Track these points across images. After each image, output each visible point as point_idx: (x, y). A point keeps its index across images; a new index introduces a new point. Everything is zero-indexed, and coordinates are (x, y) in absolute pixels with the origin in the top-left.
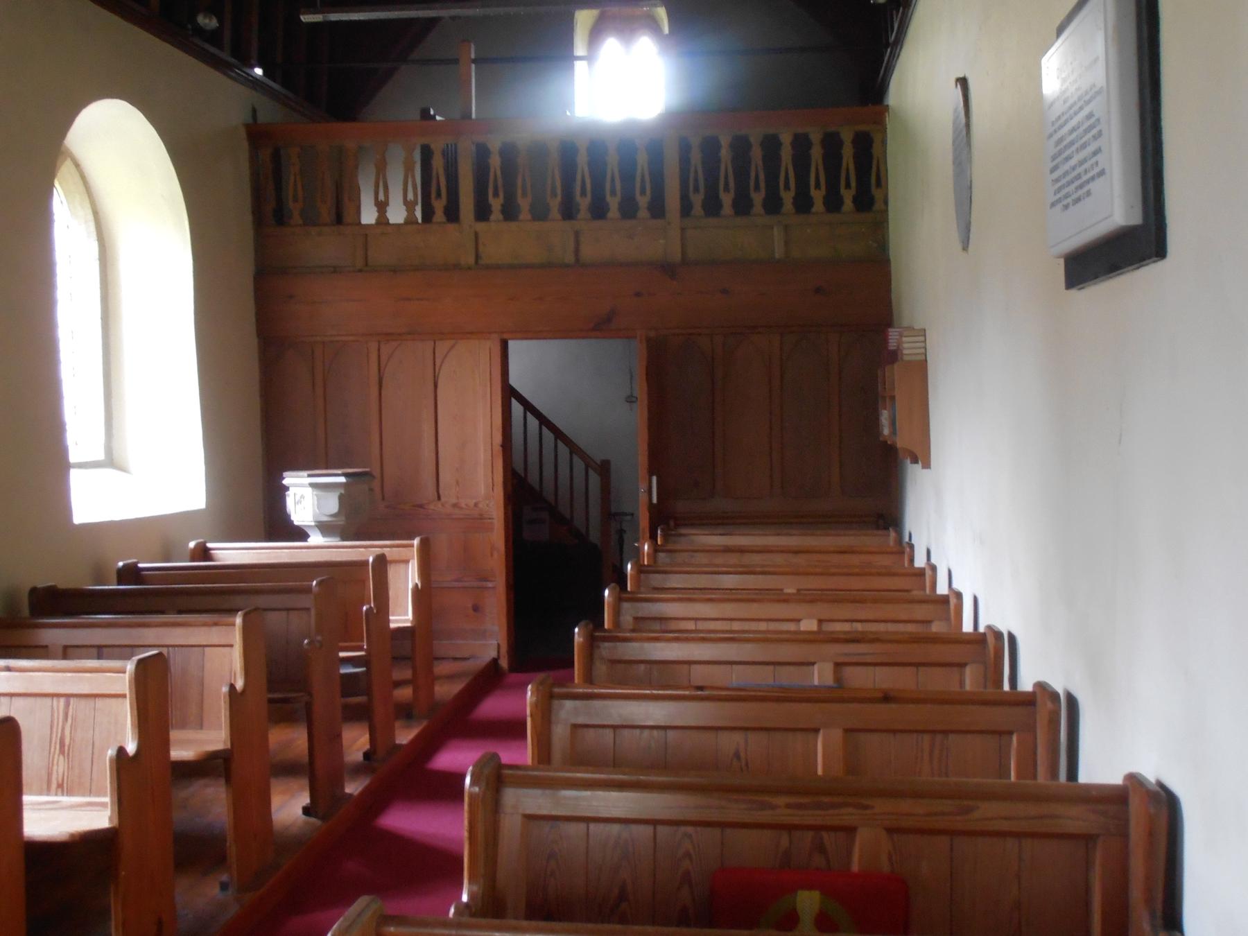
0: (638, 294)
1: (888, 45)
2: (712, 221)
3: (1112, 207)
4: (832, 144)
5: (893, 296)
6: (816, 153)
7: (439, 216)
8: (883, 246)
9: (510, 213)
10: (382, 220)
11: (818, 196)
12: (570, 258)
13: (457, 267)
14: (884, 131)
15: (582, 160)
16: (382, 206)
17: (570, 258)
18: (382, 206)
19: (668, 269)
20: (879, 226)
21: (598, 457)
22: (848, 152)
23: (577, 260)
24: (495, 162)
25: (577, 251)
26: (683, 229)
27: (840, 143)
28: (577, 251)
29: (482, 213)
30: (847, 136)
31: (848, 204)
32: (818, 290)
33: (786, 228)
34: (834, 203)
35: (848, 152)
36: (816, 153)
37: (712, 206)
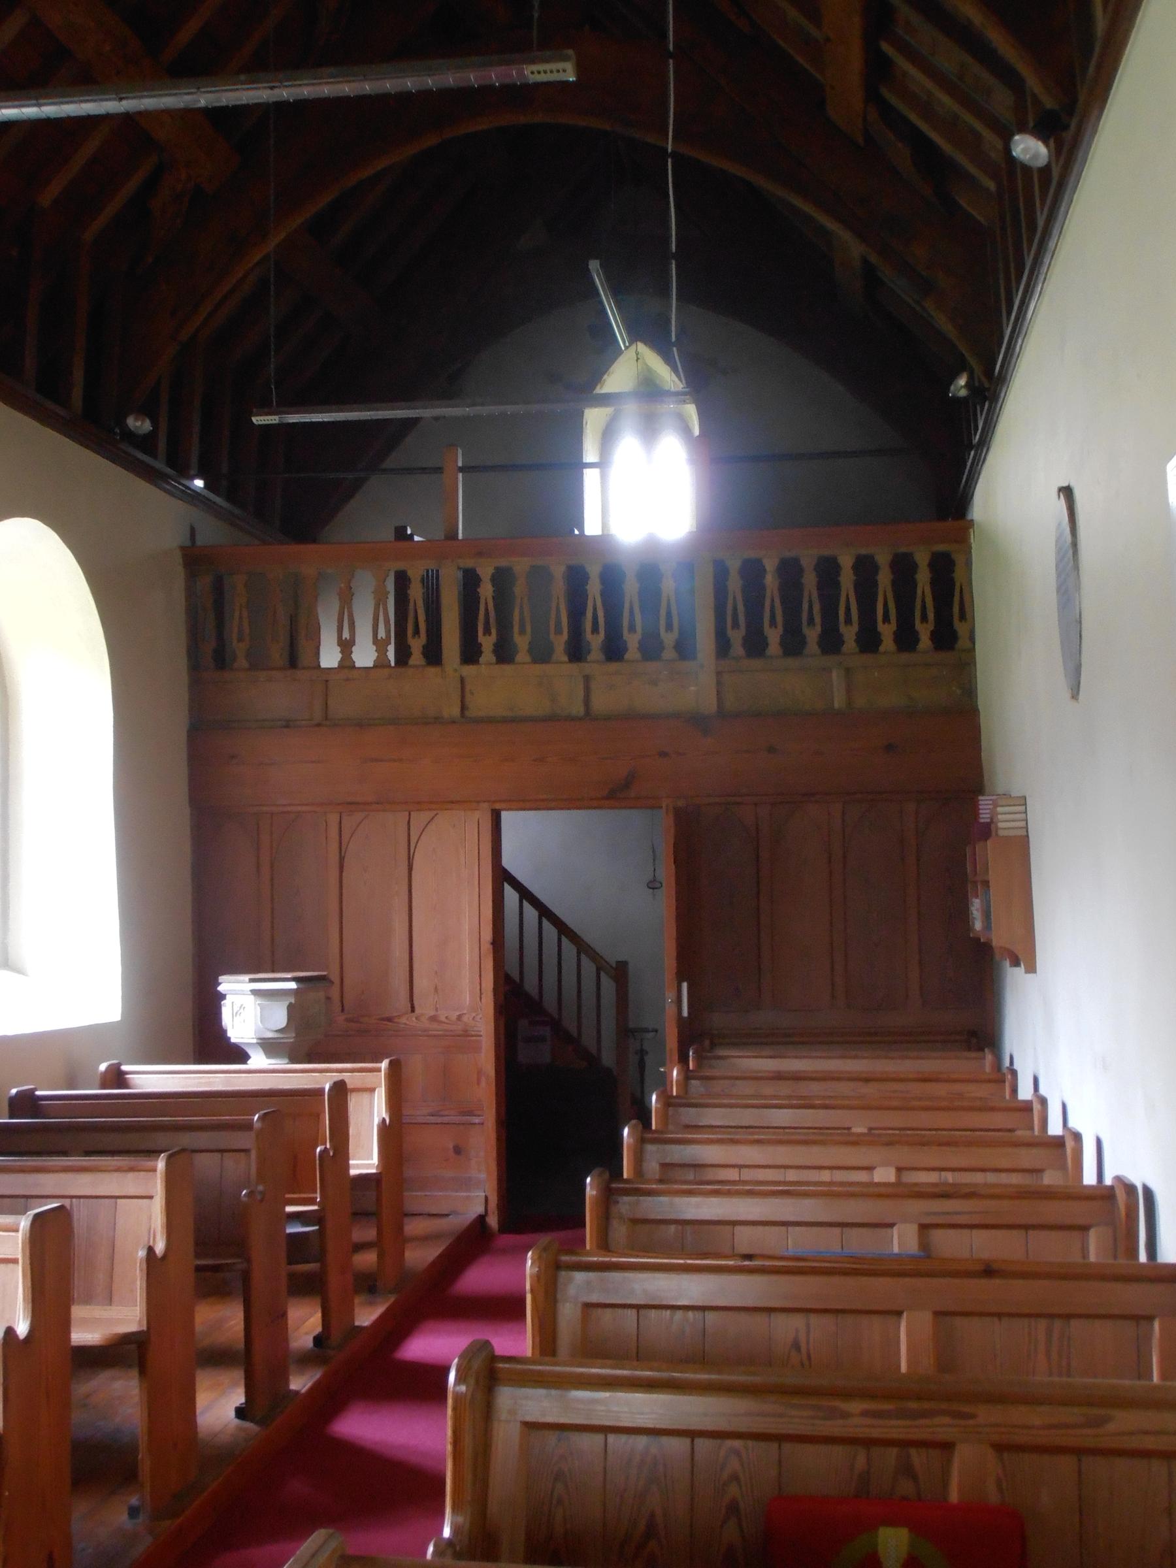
4: (903, 567)
8: (970, 691)
10: (346, 663)
12: (578, 709)
13: (438, 720)
16: (346, 646)
17: (578, 709)
18: (346, 646)
31: (925, 641)
32: (889, 748)
34: (906, 640)
36: (884, 579)
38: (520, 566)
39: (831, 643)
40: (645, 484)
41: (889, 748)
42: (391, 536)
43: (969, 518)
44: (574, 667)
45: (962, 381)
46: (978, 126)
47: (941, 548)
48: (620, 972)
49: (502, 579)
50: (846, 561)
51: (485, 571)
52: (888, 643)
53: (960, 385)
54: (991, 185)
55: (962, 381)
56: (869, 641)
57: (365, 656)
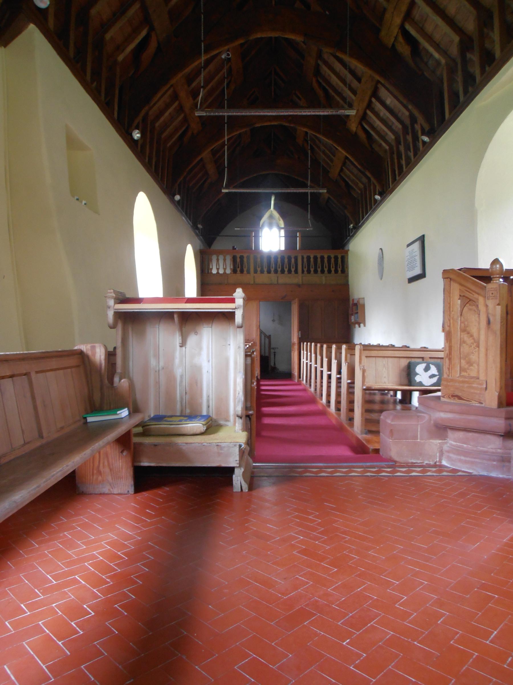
0: (292, 291)
1: (349, 236)
2: (308, 275)
3: (418, 271)
4: (336, 258)
5: (350, 294)
6: (333, 260)
7: (305, 272)
8: (347, 281)
9: (262, 272)
10: (218, 273)
11: (333, 270)
12: (276, 282)
13: (249, 284)
14: (348, 255)
15: (272, 260)
16: (218, 269)
17: (276, 282)
18: (218, 269)
19: (299, 286)
20: (347, 276)
21: (268, 334)
22: (340, 260)
23: (278, 283)
24: (259, 260)
25: (277, 281)
26: (302, 277)
27: (338, 258)
28: (277, 281)
29: (256, 272)
30: (339, 256)
31: (340, 272)
32: (333, 291)
33: (326, 277)
34: (336, 271)
35: (340, 260)
36: (333, 260)
37: (283, 272)
38: (245, 255)
39: (323, 272)
40: (271, 239)
41: (333, 291)
42: (231, 248)
43: (346, 248)
44: (275, 275)
45: (352, 226)
46: (358, 181)
47: (343, 254)
48: (269, 337)
49: (242, 258)
50: (312, 257)
51: (238, 256)
52: (333, 272)
53: (137, 135)
54: (359, 192)
55: (352, 226)
56: (330, 271)
57: (228, 271)
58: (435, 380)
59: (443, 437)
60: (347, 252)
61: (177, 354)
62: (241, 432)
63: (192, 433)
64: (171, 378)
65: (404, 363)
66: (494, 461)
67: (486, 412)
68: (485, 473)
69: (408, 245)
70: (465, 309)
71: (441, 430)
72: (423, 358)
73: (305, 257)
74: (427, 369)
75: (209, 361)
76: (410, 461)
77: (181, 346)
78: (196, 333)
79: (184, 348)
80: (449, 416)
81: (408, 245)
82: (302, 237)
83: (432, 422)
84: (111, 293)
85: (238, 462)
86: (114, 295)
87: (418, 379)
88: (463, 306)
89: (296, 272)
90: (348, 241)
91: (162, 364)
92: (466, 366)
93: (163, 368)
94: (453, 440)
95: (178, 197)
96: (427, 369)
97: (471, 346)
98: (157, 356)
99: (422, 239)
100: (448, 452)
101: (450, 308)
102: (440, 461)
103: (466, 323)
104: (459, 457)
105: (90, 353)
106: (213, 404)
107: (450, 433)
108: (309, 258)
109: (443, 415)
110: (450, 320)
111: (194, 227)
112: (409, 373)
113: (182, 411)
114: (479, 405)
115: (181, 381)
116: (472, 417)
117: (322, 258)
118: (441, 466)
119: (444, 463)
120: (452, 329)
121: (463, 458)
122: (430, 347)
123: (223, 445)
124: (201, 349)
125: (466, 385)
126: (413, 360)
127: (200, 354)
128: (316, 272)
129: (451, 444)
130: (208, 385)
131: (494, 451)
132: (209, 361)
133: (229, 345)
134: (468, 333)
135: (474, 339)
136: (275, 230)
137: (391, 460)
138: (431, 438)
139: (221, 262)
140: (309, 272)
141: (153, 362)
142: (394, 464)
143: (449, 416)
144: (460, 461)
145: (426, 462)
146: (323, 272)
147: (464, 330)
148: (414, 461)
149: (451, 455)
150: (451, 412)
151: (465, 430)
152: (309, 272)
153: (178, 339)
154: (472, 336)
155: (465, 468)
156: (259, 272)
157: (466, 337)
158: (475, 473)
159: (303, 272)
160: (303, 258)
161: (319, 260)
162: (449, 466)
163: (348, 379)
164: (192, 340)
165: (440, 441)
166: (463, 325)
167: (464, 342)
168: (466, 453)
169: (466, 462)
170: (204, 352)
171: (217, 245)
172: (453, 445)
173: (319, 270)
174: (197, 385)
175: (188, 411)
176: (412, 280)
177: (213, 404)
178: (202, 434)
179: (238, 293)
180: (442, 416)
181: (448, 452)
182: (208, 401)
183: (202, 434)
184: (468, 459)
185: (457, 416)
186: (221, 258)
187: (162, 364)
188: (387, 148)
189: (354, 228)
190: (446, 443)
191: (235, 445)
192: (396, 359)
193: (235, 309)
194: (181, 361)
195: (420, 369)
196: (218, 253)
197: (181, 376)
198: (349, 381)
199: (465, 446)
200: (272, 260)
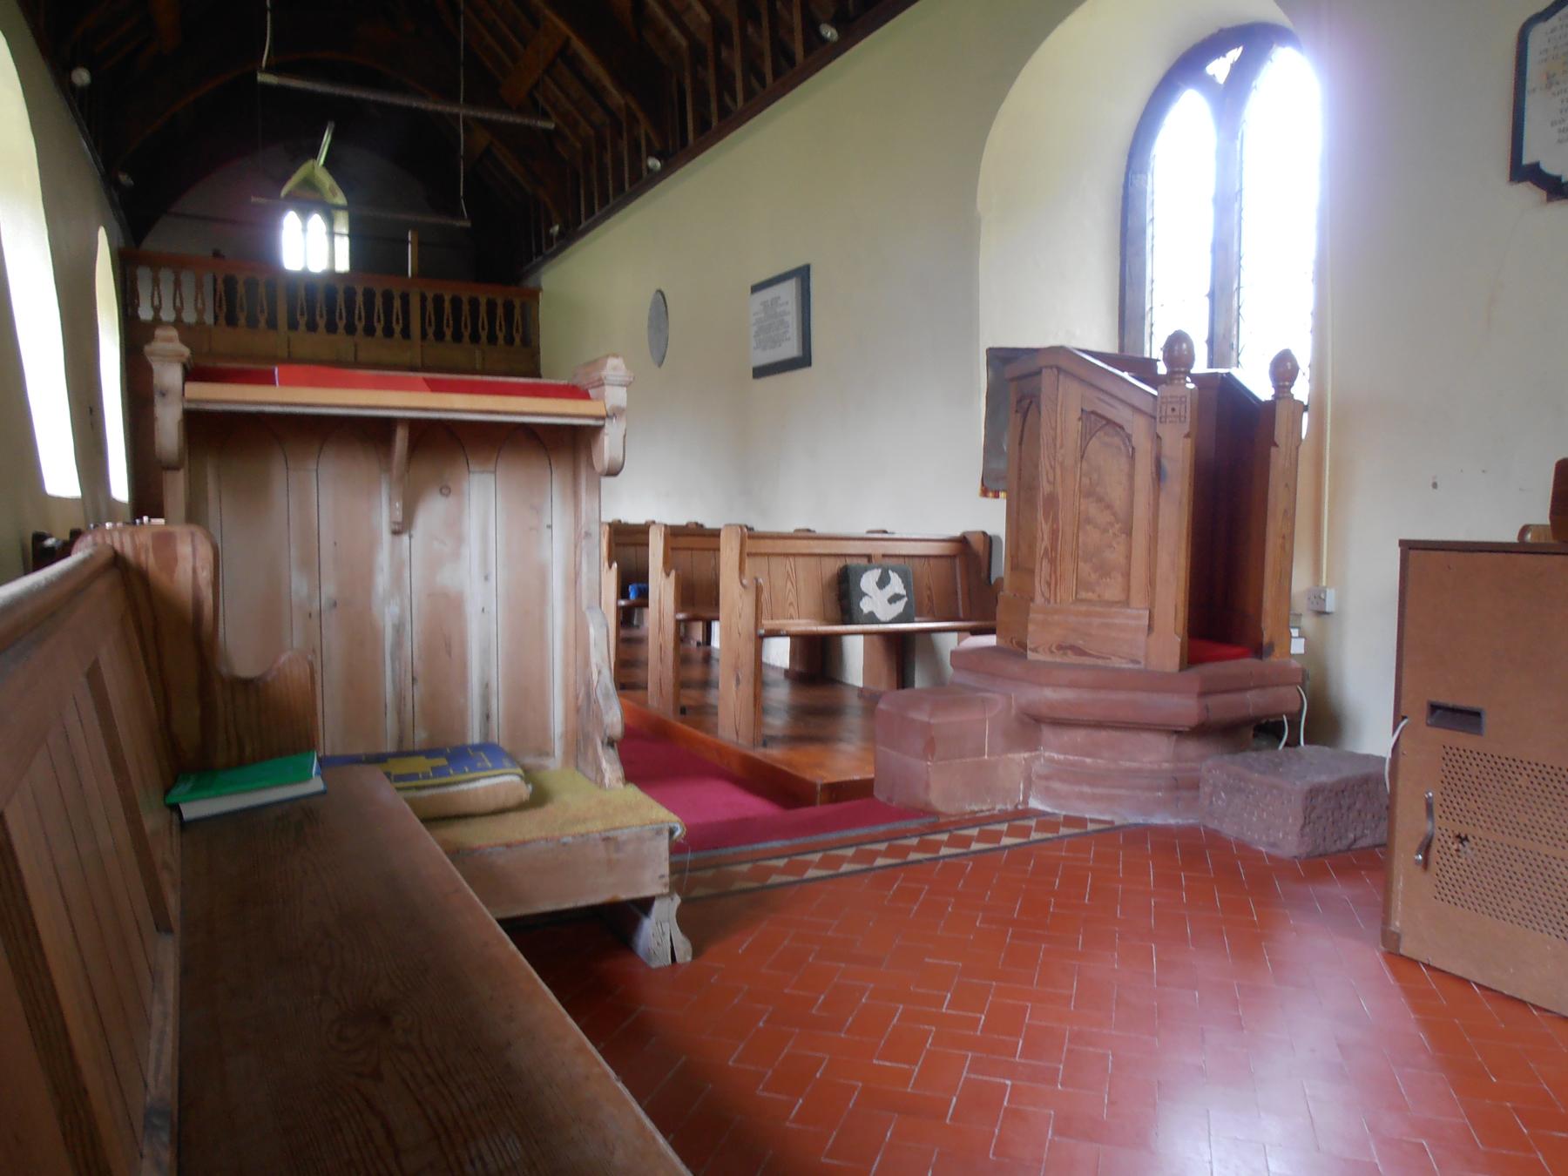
3: (791, 349)
18: (157, 310)
29: (293, 326)
36: (500, 311)
39: (475, 338)
43: (530, 283)
50: (447, 298)
52: (501, 341)
57: (209, 319)
58: (899, 607)
59: (1031, 743)
60: (534, 294)
61: (383, 558)
62: (621, 785)
63: (492, 806)
64: (362, 634)
65: (832, 567)
66: (1159, 789)
67: (1153, 681)
68: (1140, 820)
69: (756, 288)
70: (1094, 444)
71: (1032, 725)
72: (869, 557)
73: (430, 296)
74: (883, 582)
75: (486, 578)
76: (968, 808)
77: (396, 533)
78: (445, 491)
79: (405, 538)
80: (1068, 695)
81: (756, 288)
82: (421, 245)
83: (1013, 712)
84: (170, 340)
85: (667, 880)
86: (186, 351)
87: (866, 606)
88: (1086, 436)
89: (406, 333)
90: (538, 266)
91: (329, 589)
92: (1094, 577)
93: (335, 604)
94: (1053, 750)
95: (82, 77)
96: (883, 582)
97: (1105, 531)
98: (311, 564)
99: (802, 275)
100: (1047, 778)
101: (1055, 439)
102: (1025, 802)
103: (1095, 476)
104: (1077, 789)
105: (150, 561)
106: (498, 706)
107: (1047, 733)
108: (439, 300)
109: (1050, 694)
110: (1053, 468)
111: (109, 181)
112: (842, 596)
113: (401, 740)
114: (1131, 666)
115: (398, 644)
116: (1121, 696)
117: (474, 303)
118: (1026, 813)
119: (1034, 804)
120: (1060, 491)
121: (1086, 789)
122: (821, 528)
123: (622, 835)
124: (460, 540)
125: (1096, 621)
126: (849, 561)
127: (456, 555)
128: (457, 337)
129: (1052, 760)
130: (485, 652)
131: (1156, 767)
132: (486, 578)
133: (550, 527)
134: (1100, 500)
135: (1114, 514)
136: (317, 221)
137: (925, 811)
138: (1010, 749)
139: (167, 291)
140: (439, 336)
141: (298, 585)
142: (930, 820)
143: (1068, 695)
144: (1081, 796)
145: (999, 807)
146: (475, 338)
147: (1089, 493)
148: (976, 808)
149: (1056, 785)
150: (1072, 685)
151: (1099, 725)
152: (439, 336)
153: (384, 512)
154: (1109, 507)
155: (1096, 813)
156: (302, 327)
157: (1092, 509)
158: (1118, 822)
159: (424, 335)
160: (423, 299)
161: (466, 308)
162: (1048, 810)
163: (677, 611)
164: (433, 512)
165: (1026, 755)
166: (1086, 481)
167: (1088, 521)
168: (1094, 778)
169: (1094, 798)
170: (472, 549)
171: (151, 244)
172: (1058, 762)
173: (466, 334)
174: (449, 653)
175: (420, 737)
176: (761, 372)
177: (498, 706)
178: (522, 807)
179: (615, 369)
180: (1049, 696)
181: (1047, 778)
182: (486, 699)
183: (522, 807)
184: (1099, 791)
185: (1087, 695)
186: (188, 280)
187: (329, 589)
188: (684, 43)
189: (561, 234)
190: (1038, 758)
191: (659, 832)
192: (813, 561)
193: (603, 418)
194: (397, 579)
195: (868, 581)
196: (178, 264)
197: (399, 629)
198: (681, 616)
199: (1088, 760)
200: (321, 297)
